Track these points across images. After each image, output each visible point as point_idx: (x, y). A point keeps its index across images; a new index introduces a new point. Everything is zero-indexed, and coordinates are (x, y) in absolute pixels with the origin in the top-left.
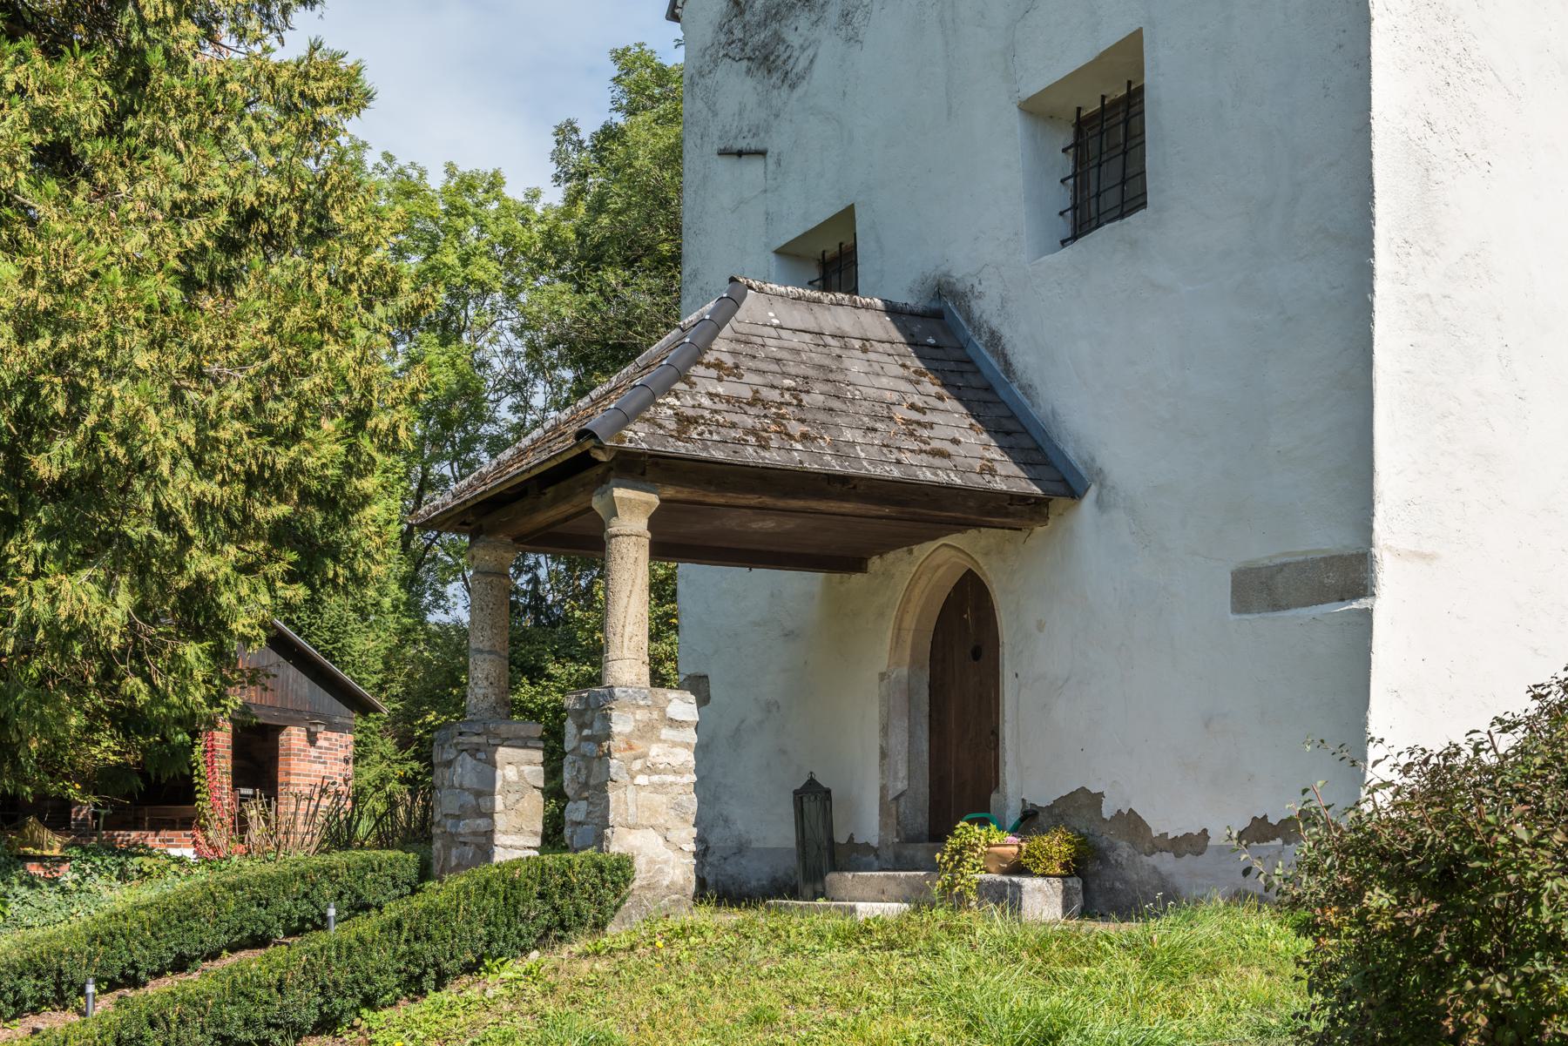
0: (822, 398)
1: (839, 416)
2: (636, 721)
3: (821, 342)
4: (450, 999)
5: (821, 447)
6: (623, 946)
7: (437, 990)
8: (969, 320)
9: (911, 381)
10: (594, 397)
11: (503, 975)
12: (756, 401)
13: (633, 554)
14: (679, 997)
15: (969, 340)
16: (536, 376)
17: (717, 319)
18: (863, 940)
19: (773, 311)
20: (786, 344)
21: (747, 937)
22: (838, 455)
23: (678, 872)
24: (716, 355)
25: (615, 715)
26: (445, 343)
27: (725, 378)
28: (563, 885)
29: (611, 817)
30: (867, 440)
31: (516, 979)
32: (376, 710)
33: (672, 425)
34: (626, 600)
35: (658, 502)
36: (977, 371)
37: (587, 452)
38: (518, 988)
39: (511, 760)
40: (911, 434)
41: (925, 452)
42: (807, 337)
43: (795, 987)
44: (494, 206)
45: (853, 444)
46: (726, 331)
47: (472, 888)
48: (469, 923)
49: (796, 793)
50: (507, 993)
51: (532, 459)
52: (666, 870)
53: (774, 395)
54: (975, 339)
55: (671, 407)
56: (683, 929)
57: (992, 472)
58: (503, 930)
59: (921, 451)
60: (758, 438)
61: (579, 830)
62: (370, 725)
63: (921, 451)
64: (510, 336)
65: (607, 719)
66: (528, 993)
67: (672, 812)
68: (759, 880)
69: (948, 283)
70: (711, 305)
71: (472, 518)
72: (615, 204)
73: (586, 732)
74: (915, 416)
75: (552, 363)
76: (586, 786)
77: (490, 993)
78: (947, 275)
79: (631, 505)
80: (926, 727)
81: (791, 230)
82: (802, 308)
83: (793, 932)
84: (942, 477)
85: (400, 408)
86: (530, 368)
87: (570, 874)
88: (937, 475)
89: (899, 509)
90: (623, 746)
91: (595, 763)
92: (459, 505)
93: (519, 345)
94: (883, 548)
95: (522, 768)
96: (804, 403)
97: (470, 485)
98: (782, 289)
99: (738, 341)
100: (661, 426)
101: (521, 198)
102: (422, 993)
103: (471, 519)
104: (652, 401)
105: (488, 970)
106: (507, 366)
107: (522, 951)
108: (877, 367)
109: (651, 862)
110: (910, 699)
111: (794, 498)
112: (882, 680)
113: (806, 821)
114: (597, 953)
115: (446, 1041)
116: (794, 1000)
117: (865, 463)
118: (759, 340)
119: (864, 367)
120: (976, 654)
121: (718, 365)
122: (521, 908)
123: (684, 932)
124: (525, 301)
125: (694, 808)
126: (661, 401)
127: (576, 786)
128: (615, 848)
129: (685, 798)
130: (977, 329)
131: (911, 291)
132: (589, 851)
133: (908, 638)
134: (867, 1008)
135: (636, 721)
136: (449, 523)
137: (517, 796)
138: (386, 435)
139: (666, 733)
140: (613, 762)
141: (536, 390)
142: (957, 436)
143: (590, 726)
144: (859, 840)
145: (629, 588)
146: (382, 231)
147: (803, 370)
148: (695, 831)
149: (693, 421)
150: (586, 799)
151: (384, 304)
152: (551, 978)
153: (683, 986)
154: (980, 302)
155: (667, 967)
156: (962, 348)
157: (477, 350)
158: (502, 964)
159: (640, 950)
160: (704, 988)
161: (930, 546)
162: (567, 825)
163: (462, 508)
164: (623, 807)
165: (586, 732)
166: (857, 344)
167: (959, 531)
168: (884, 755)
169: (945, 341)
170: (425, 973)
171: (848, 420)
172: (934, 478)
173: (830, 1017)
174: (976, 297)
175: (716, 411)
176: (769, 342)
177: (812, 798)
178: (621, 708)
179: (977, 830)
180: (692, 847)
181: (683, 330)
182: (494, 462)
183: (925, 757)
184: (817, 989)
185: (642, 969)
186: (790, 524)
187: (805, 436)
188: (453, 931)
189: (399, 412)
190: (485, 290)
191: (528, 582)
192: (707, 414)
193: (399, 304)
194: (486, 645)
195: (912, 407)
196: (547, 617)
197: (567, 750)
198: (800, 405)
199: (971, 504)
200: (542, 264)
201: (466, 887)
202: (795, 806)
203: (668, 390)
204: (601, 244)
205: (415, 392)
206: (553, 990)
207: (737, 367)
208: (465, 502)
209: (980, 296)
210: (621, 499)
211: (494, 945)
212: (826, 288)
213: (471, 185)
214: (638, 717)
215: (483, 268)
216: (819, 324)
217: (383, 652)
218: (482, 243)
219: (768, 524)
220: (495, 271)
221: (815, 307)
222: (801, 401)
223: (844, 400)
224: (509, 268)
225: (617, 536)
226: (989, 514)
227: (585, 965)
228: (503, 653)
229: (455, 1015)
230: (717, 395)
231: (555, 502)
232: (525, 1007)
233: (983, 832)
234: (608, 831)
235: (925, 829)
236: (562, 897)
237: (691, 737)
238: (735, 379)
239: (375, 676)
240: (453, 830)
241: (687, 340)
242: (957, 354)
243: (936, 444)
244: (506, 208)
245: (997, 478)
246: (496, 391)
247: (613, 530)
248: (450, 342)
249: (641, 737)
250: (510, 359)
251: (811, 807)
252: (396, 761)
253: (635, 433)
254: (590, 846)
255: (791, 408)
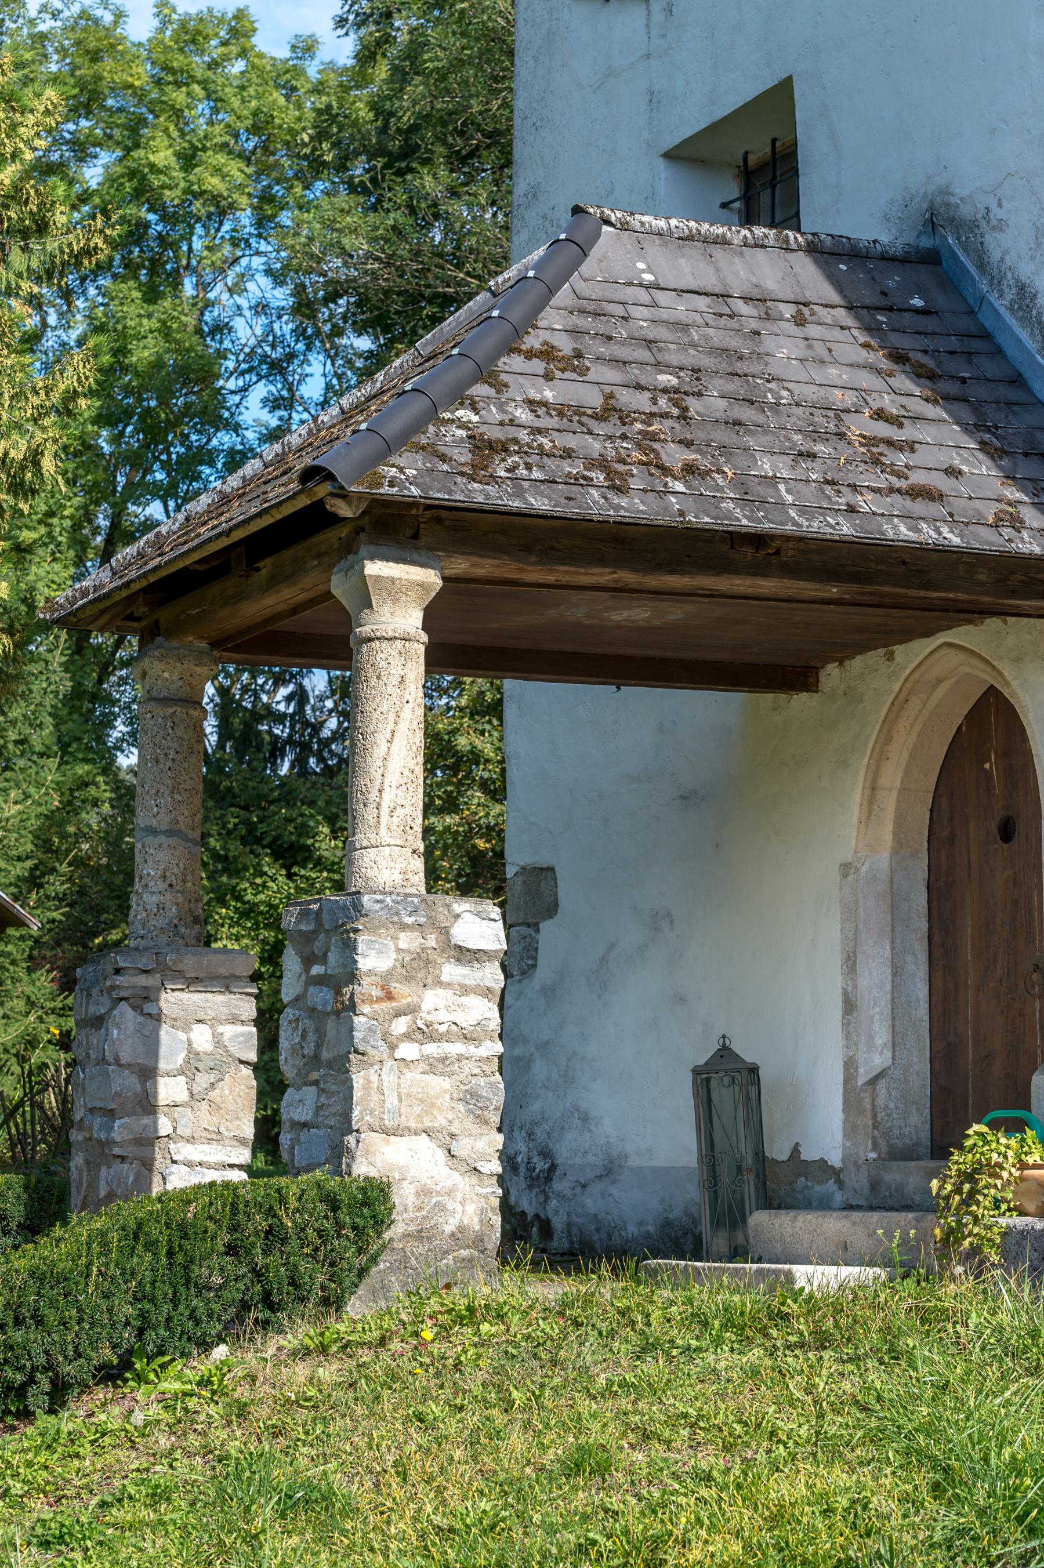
0: (722, 403)
1: (751, 433)
2: (399, 950)
3: (726, 310)
4: (71, 1426)
5: (718, 488)
6: (367, 1338)
7: (52, 1411)
8: (982, 267)
9: (879, 372)
10: (346, 406)
11: (165, 1385)
12: (609, 411)
13: (397, 670)
14: (452, 1426)
15: (982, 299)
16: (309, 348)
17: (548, 276)
18: (774, 1332)
19: (643, 259)
20: (665, 315)
21: (578, 1325)
22: (745, 500)
23: (471, 1208)
24: (544, 335)
25: (362, 941)
26: (152, 295)
27: (558, 374)
28: (269, 1232)
29: (356, 1114)
30: (799, 474)
31: (185, 1394)
32: (20, 923)
33: (463, 456)
34: (384, 746)
35: (440, 583)
36: (998, 352)
37: (320, 503)
38: (186, 1410)
39: (201, 1015)
40: (876, 461)
41: (899, 491)
42: (702, 303)
43: (650, 1410)
44: (239, 66)
45: (773, 481)
46: (563, 296)
47: (114, 1236)
48: (106, 1296)
49: (696, 1072)
50: (167, 1417)
51: (237, 513)
52: (450, 1205)
53: (641, 401)
54: (993, 297)
55: (463, 426)
56: (471, 1310)
57: (1016, 523)
58: (166, 1308)
59: (892, 490)
60: (609, 472)
61: (303, 1136)
62: (10, 948)
63: (892, 490)
64: (265, 281)
65: (350, 947)
66: (202, 1417)
67: (461, 1107)
68: (640, 1223)
69: (948, 205)
70: (541, 252)
71: (143, 609)
72: (433, 60)
73: (316, 970)
74: (883, 430)
75: (334, 326)
76: (315, 1061)
77: (138, 1418)
78: (945, 191)
79: (394, 589)
80: (923, 957)
81: (794, 79)
82: (693, 252)
83: (656, 1315)
84: (928, 534)
85: (46, 422)
86: (299, 333)
87: (282, 1213)
88: (918, 531)
89: (855, 587)
90: (376, 993)
91: (331, 1024)
92: (119, 588)
93: (281, 297)
94: (843, 653)
95: (221, 1029)
96: (692, 413)
97: (141, 555)
98: (662, 223)
99: (583, 312)
100: (444, 458)
101: (283, 53)
102: (26, 1415)
103: (141, 609)
104: (432, 416)
105: (140, 1378)
106: (259, 331)
107: (199, 1345)
108: (820, 349)
109: (424, 1192)
110: (893, 908)
111: (673, 572)
112: (845, 876)
113: (715, 1119)
114: (323, 1349)
115: (59, 1499)
116: (646, 1436)
117: (793, 513)
118: (619, 311)
119: (798, 350)
120: (1007, 831)
121: (547, 353)
122: (196, 1270)
123: (470, 1315)
124: (289, 223)
125: (499, 1099)
126: (447, 415)
127: (299, 1062)
128: (361, 1169)
129: (482, 1081)
130: (997, 282)
131: (886, 218)
132: (318, 1173)
133: (889, 803)
134: (769, 1451)
135: (399, 950)
136: (106, 617)
137: (212, 1077)
138: (23, 468)
139: (451, 971)
140: (359, 1021)
141: (308, 370)
142: (957, 462)
143: (323, 960)
144: (809, 1154)
145: (391, 726)
146: (22, 130)
147: (692, 358)
148: (500, 1138)
149: (500, 448)
150: (316, 1083)
151: (25, 249)
152: (243, 1393)
153: (461, 1409)
154: (998, 235)
155: (438, 1374)
156: (971, 312)
157: (209, 304)
158: (163, 1366)
159: (395, 1345)
160: (495, 1412)
161: (922, 647)
162: (286, 1126)
163: (124, 594)
164: (375, 1097)
165: (316, 970)
166: (788, 311)
167: (970, 622)
168: (850, 1005)
169: (941, 301)
170: (32, 1380)
171: (764, 439)
172: (912, 536)
173: (704, 1465)
174: (994, 228)
175: (539, 431)
176: (636, 312)
177: (726, 1080)
178: (373, 930)
179: (1003, 1140)
180: (496, 1167)
181: (494, 295)
182: (181, 517)
183: (922, 1011)
184: (685, 1416)
185: (395, 1378)
186: (675, 613)
187: (690, 469)
188: (80, 1310)
189: (43, 429)
190: (221, 208)
191: (289, 699)
192: (524, 436)
193: (49, 248)
194: (163, 821)
195: (880, 415)
196: (321, 760)
197: (285, 1001)
198: (684, 417)
199: (981, 577)
200: (317, 166)
201: (103, 1234)
202: (696, 1095)
203: (459, 398)
204: (414, 129)
205: (71, 396)
206: (242, 1411)
207: (579, 355)
208: (127, 585)
209: (1000, 226)
210: (378, 578)
211: (150, 1335)
212: (749, 219)
213: (199, 32)
214: (403, 945)
215: (217, 171)
216: (723, 281)
217: (34, 823)
218: (218, 129)
219: (639, 613)
220: (239, 178)
221: (717, 251)
222: (687, 409)
223: (761, 406)
224: (263, 170)
225: (370, 640)
226: (1014, 594)
227: (301, 1371)
228: (191, 835)
229: (77, 1456)
230: (544, 404)
231: (274, 582)
232: (194, 1441)
233: (1013, 1142)
234: (351, 1139)
235: (925, 1134)
236: (266, 1252)
237: (492, 976)
238: (574, 376)
239: (19, 865)
240: (103, 1136)
241: (495, 313)
242: (964, 323)
243: (918, 478)
244: (260, 71)
245: (1025, 534)
246: (243, 373)
247: (365, 630)
248: (161, 296)
249: (408, 979)
250: (263, 320)
251: (724, 1096)
252: (53, 1011)
253: (401, 470)
254: (320, 1165)
255: (668, 423)
